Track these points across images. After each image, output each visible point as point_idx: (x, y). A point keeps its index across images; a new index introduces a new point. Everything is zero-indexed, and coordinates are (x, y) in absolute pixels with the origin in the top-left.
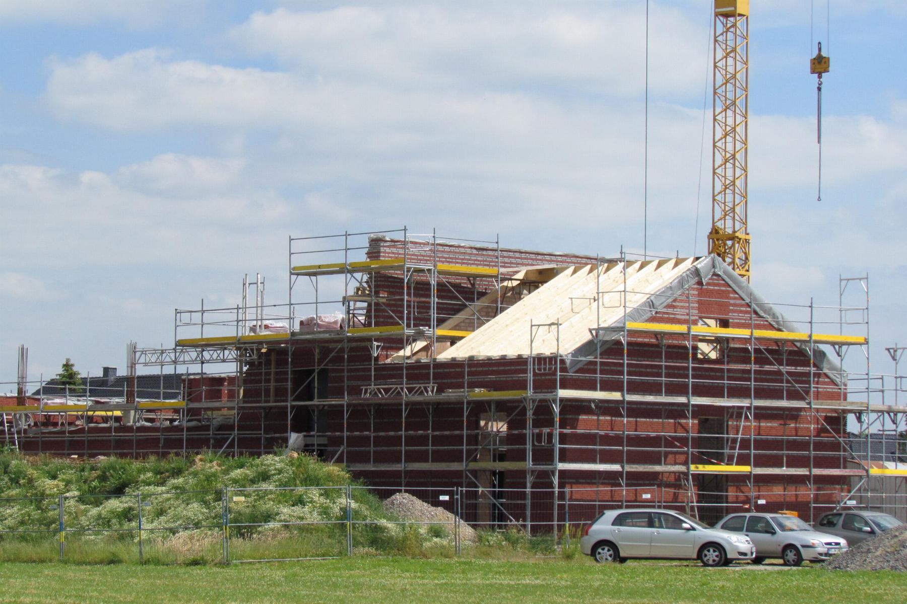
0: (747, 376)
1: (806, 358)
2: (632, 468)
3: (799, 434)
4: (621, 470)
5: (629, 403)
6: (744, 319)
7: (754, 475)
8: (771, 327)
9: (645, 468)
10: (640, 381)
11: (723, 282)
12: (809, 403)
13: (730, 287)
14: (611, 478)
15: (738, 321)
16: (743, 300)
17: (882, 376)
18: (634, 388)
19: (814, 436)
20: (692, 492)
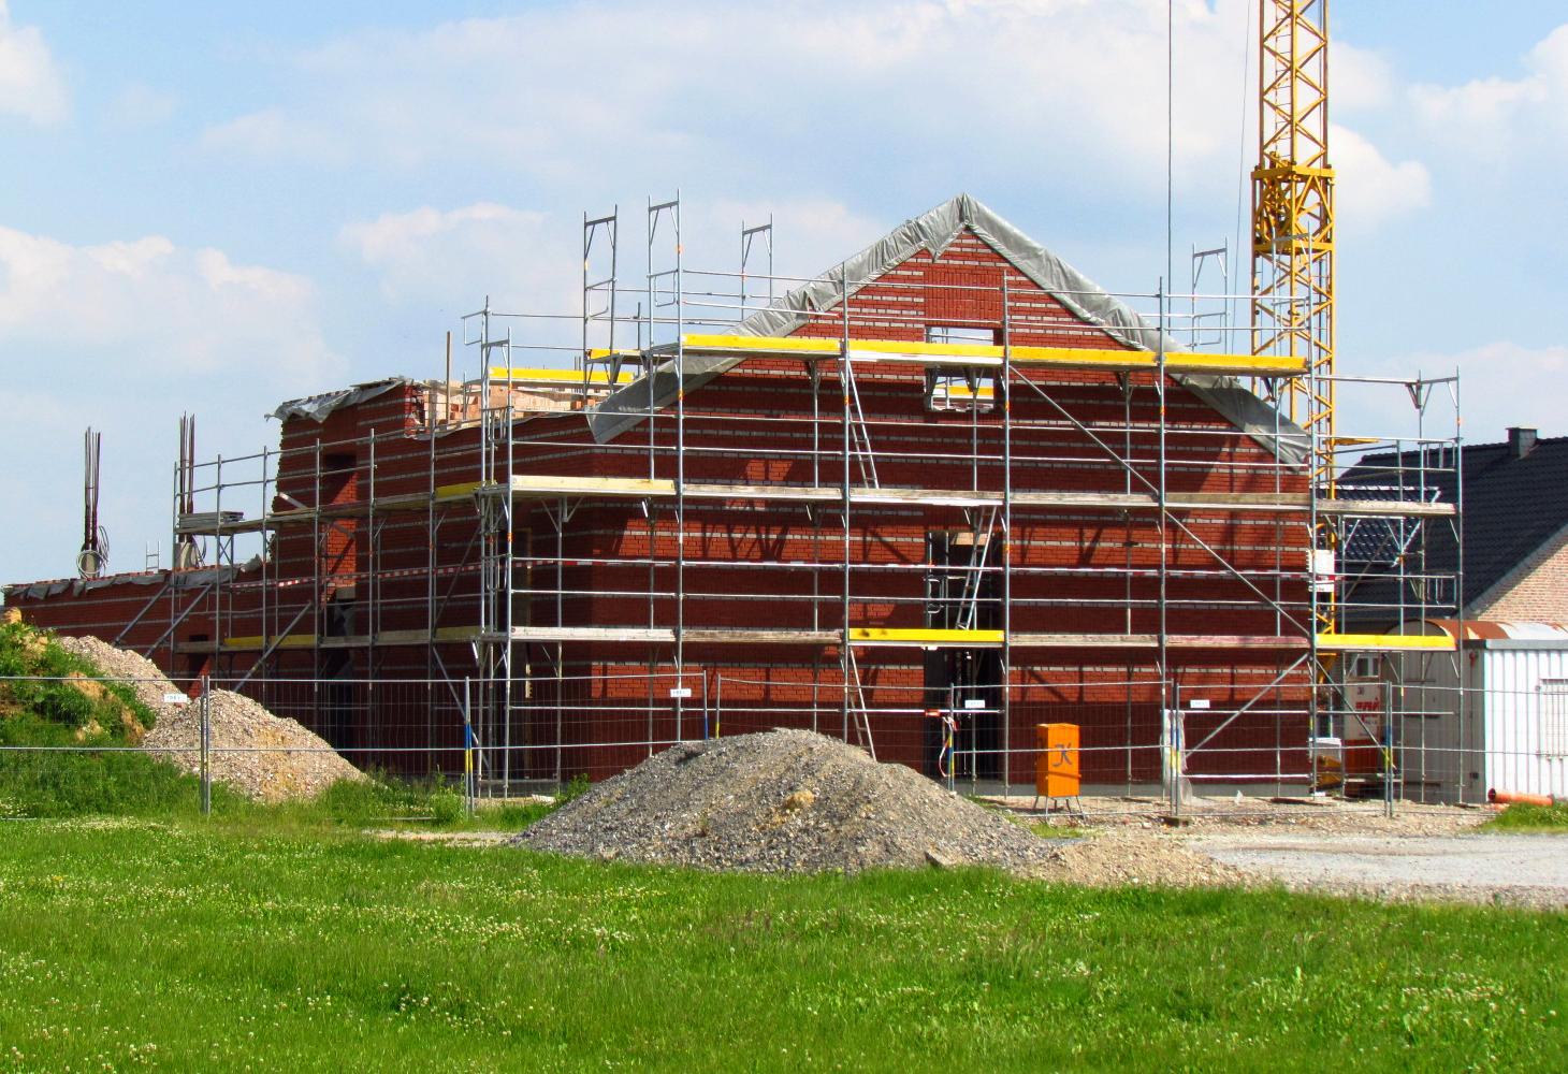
0: (995, 442)
1: (1202, 406)
2: (703, 635)
3: (710, 554)
4: (673, 640)
5: (688, 500)
6: (1042, 328)
7: (1011, 648)
8: (1111, 342)
9: (733, 636)
10: (735, 455)
11: (989, 251)
12: (1158, 499)
13: (1006, 260)
14: (664, 651)
15: (1027, 331)
16: (1039, 287)
17: (1398, 441)
18: (700, 470)
19: (1168, 567)
20: (851, 684)
